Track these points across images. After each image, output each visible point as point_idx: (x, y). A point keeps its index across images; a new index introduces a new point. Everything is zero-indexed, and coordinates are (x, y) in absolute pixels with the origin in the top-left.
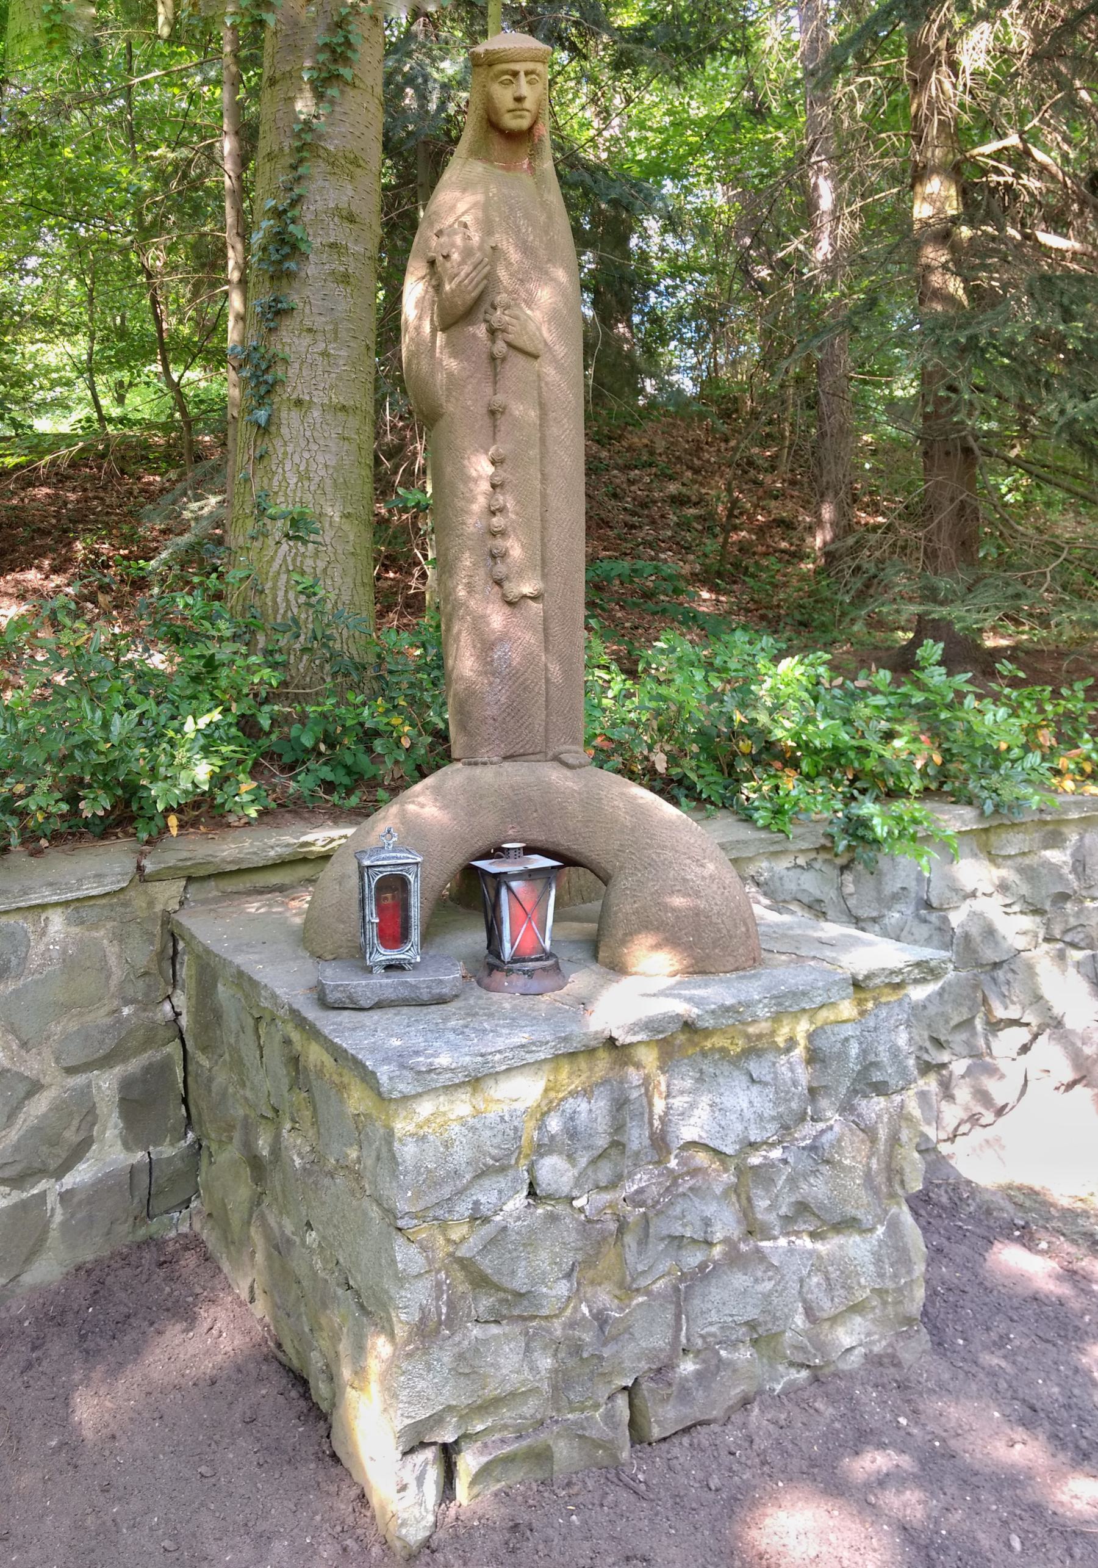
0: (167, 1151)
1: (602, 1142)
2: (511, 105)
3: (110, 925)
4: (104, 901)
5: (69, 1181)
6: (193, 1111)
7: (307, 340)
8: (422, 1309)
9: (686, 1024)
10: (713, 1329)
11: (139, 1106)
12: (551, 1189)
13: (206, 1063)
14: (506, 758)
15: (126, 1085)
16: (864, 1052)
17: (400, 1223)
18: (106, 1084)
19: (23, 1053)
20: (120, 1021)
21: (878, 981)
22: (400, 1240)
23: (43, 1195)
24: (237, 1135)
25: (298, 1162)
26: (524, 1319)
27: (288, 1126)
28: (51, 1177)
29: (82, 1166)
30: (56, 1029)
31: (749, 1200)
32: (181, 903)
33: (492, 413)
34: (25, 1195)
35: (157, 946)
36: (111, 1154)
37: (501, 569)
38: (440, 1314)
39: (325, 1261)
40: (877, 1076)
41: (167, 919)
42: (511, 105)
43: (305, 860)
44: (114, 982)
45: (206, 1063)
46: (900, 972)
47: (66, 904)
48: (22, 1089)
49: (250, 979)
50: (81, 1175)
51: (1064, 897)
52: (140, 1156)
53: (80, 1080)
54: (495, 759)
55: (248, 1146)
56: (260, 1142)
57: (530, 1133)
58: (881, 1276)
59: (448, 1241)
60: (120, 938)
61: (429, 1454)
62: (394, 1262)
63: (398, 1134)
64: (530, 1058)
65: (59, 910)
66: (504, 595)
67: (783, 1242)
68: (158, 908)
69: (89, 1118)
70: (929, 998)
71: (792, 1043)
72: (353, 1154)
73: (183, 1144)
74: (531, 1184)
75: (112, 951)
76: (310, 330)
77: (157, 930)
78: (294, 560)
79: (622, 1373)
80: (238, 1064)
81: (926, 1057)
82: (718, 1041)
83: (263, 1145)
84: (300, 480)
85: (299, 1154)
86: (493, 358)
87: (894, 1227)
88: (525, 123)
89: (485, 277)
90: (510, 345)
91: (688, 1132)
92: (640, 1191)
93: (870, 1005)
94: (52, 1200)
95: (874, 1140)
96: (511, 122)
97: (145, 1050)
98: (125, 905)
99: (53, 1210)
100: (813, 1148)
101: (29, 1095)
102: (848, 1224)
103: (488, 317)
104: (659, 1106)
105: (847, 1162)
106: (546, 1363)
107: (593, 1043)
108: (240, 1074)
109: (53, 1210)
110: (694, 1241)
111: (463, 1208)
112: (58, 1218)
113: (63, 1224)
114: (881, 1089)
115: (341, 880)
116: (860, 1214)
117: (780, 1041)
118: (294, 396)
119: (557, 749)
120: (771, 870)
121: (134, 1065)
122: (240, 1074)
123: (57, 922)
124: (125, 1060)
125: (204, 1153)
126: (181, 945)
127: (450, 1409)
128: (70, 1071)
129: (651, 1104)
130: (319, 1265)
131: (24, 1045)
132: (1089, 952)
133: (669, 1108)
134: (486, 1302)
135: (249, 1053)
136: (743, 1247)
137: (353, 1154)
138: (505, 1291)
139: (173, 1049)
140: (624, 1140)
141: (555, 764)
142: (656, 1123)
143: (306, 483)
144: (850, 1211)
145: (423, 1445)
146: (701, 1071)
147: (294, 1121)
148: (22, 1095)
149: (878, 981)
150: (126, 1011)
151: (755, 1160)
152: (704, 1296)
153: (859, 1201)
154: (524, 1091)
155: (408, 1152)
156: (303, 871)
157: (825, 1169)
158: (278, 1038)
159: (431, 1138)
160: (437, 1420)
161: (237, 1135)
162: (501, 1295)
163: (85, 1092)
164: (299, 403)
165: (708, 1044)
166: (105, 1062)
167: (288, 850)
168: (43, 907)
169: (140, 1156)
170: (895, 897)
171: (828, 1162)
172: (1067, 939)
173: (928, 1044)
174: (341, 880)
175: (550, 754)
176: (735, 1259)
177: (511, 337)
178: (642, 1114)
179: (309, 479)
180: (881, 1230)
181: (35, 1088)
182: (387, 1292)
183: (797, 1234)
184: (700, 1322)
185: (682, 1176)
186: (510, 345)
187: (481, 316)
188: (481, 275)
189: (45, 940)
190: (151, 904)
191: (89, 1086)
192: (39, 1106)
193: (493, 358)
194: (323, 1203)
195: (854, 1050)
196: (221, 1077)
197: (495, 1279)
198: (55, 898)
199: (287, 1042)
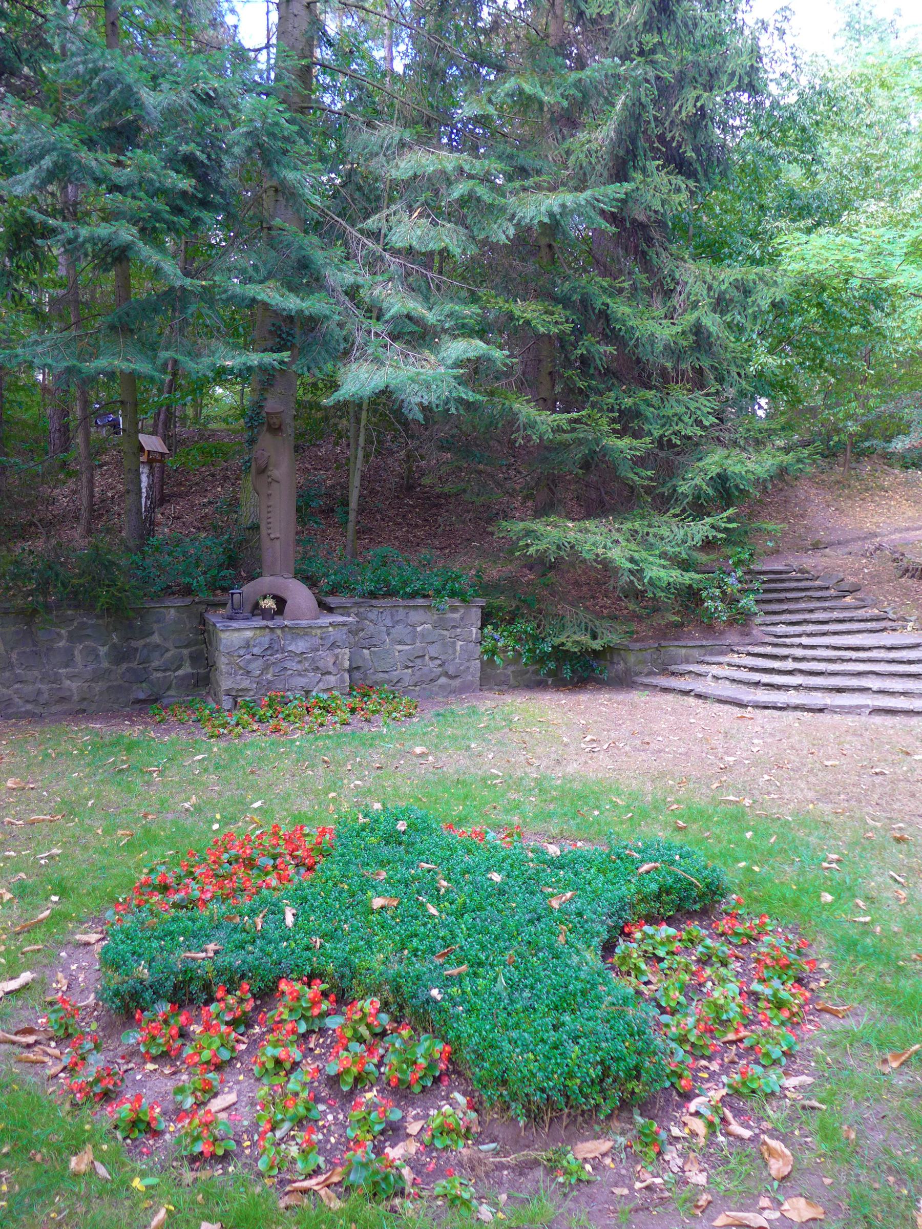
5: (177, 674)
15: (191, 653)
36: (187, 669)
50: (180, 672)
102: (329, 673)
121: (193, 649)
123: (172, 611)
155: (224, 641)
166: (186, 647)
181: (167, 650)
192: (168, 655)
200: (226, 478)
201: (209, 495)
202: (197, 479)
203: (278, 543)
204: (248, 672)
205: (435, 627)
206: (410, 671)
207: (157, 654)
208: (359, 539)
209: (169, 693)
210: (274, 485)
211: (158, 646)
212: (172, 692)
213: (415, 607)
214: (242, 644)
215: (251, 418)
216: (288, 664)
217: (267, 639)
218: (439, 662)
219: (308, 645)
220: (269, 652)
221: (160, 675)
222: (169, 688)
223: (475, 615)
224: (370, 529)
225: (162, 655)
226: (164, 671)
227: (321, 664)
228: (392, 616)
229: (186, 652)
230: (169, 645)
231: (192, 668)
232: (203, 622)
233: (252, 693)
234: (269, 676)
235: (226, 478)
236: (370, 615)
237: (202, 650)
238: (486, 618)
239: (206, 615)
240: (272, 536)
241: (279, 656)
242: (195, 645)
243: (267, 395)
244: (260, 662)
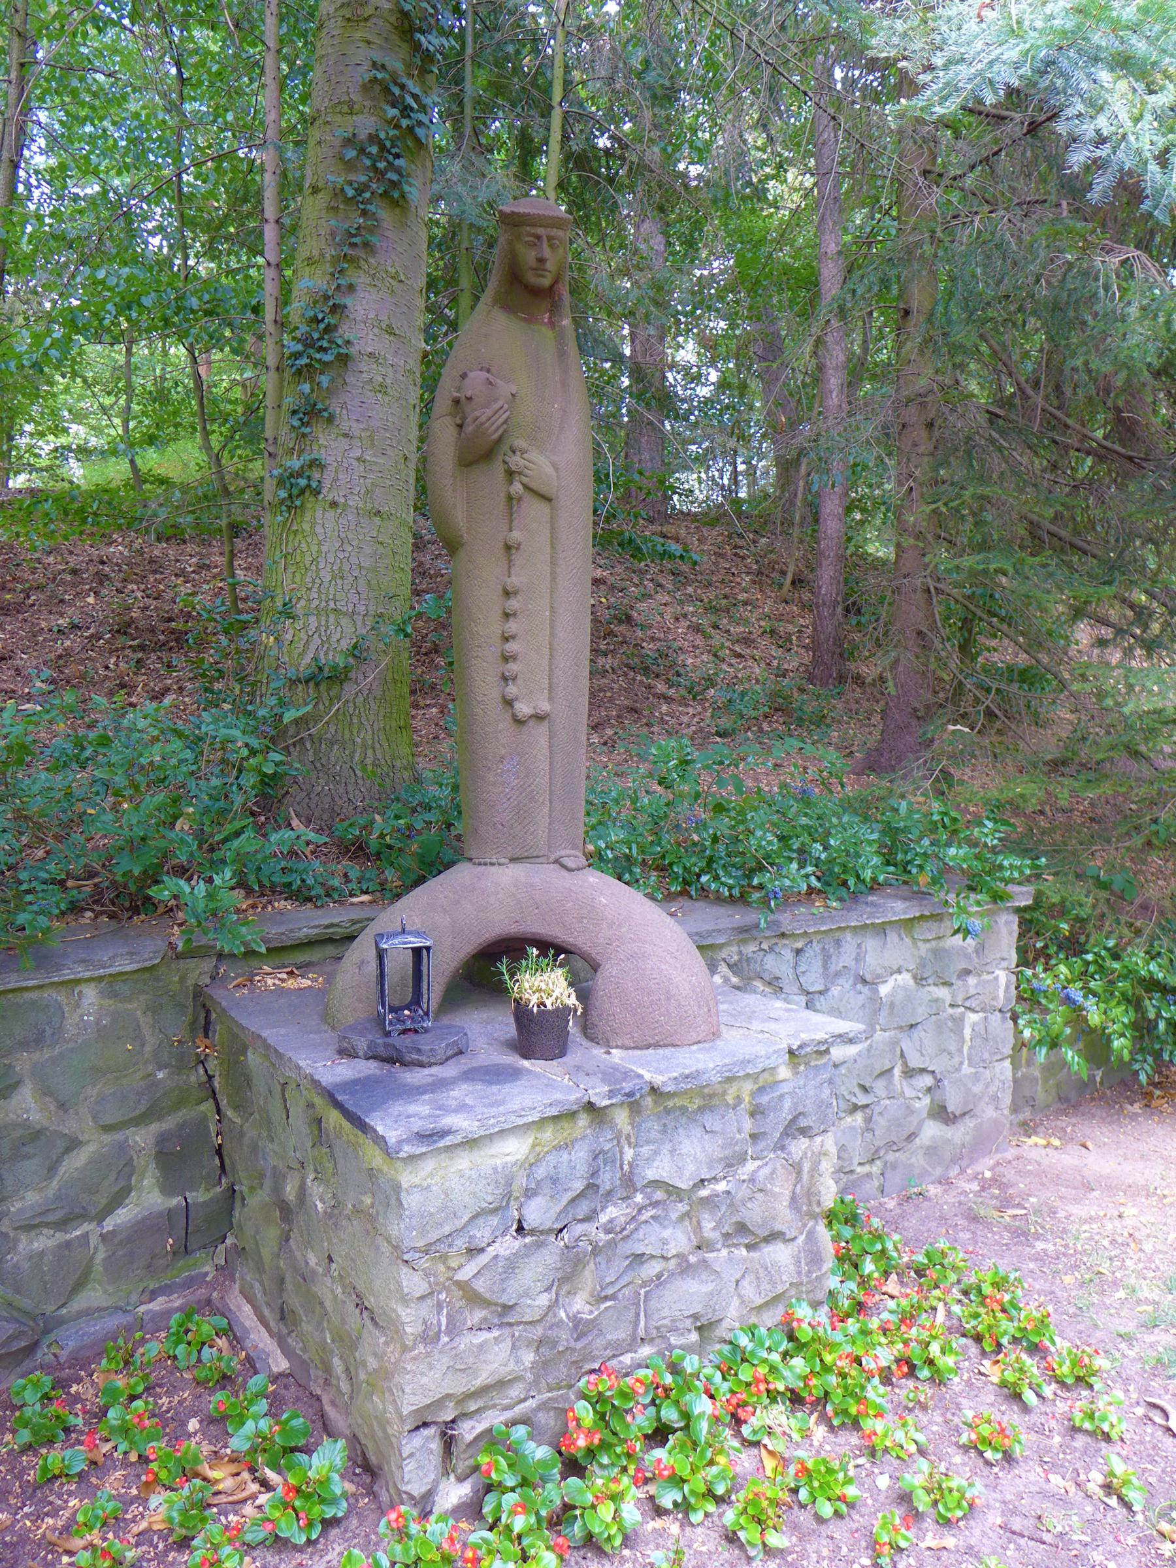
0: (199, 1196)
1: (579, 1186)
2: (534, 264)
3: (142, 998)
4: (136, 976)
5: (109, 1225)
6: (227, 1161)
7: (344, 443)
8: (425, 1322)
9: (653, 1088)
10: (665, 1322)
11: (173, 1160)
12: (535, 1224)
13: (238, 1120)
14: (512, 860)
15: (162, 1139)
16: (795, 1105)
17: (406, 1257)
18: (142, 1138)
19: (61, 1113)
20: (157, 1084)
21: (808, 1049)
22: (405, 1270)
23: (86, 1235)
24: (268, 1183)
25: (320, 1205)
26: (511, 1325)
27: (311, 1177)
28: (92, 1220)
29: (121, 1211)
30: (93, 1092)
31: (699, 1223)
32: (213, 978)
33: (508, 548)
34: (68, 1237)
35: (190, 1018)
36: (149, 1198)
37: (512, 690)
38: (440, 1325)
39: (344, 1287)
40: (803, 1122)
41: (198, 992)
42: (534, 264)
43: (331, 940)
44: (148, 1048)
45: (238, 1120)
46: (826, 1042)
47: (100, 979)
48: (61, 1144)
49: (276, 1051)
50: (122, 1216)
51: (967, 972)
52: (176, 1201)
53: (118, 1136)
54: (503, 860)
55: (277, 1190)
56: (288, 1188)
57: (521, 1182)
58: (799, 1273)
59: (449, 1268)
60: (153, 1009)
61: (431, 1431)
62: (401, 1287)
63: (405, 1185)
64: (520, 1121)
65: (93, 985)
66: (514, 716)
67: (724, 1252)
68: (190, 982)
69: (127, 1169)
70: (859, 1054)
71: (739, 1099)
72: (368, 1200)
73: (218, 1189)
74: (519, 1221)
75: (145, 1021)
76: (346, 435)
77: (190, 1002)
78: (326, 653)
79: (593, 1360)
80: (267, 1122)
81: (854, 1100)
82: (678, 1102)
83: (290, 1191)
84: (334, 578)
85: (321, 1200)
86: (510, 498)
87: (811, 1236)
88: (546, 282)
89: (505, 422)
90: (525, 486)
91: (651, 1174)
92: (611, 1221)
93: (802, 1068)
94: (94, 1240)
95: (799, 1173)
96: (532, 279)
97: (179, 1109)
98: (157, 979)
99: (96, 1248)
100: (752, 1180)
101: (68, 1150)
102: (774, 1236)
103: (507, 459)
104: (629, 1154)
105: (777, 1190)
106: (528, 1357)
107: (575, 1107)
108: (269, 1130)
109: (96, 1248)
110: (652, 1257)
111: (461, 1243)
112: (101, 1256)
113: (104, 1260)
114: (804, 1132)
115: (361, 964)
116: (784, 1228)
117: (730, 1099)
118: (330, 498)
119: (559, 854)
120: (740, 953)
121: (169, 1124)
122: (269, 1130)
123: (90, 994)
124: (160, 1118)
125: (238, 1195)
126: (214, 1016)
127: (448, 1396)
128: (108, 1129)
129: (621, 1153)
130: (339, 1290)
131: (62, 1106)
132: (981, 1015)
133: (637, 1155)
134: (479, 1315)
135: (277, 1113)
136: (692, 1259)
137: (368, 1200)
138: (496, 1304)
139: (208, 1107)
140: (598, 1182)
141: (557, 866)
142: (626, 1167)
143: (339, 582)
144: (778, 1227)
145: (425, 1425)
146: (665, 1125)
147: (316, 1171)
148: (61, 1150)
149: (808, 1049)
150: (160, 1075)
151: (704, 1193)
152: (659, 1297)
153: (785, 1218)
154: (515, 1149)
155: (412, 1201)
156: (330, 950)
157: (760, 1196)
158: (302, 1103)
159: (434, 1188)
160: (439, 1404)
161: (268, 1183)
162: (493, 1308)
163: (122, 1147)
164: (334, 504)
165: (670, 1104)
166: (140, 1120)
167: (316, 931)
168: (78, 982)
169: (176, 1201)
170: (838, 974)
171: (761, 1190)
172: (967, 1004)
173: (857, 1090)
174: (361, 964)
175: (552, 859)
176: (685, 1268)
177: (525, 480)
178: (614, 1161)
179: (342, 578)
180: (801, 1239)
181: (74, 1144)
182: (395, 1311)
183: (736, 1246)
184: (656, 1317)
185: (645, 1207)
186: (525, 486)
187: (501, 458)
188: (501, 420)
189: (80, 1011)
190: (183, 979)
191: (126, 1141)
192: (79, 1159)
193: (510, 498)
194: (342, 1241)
195: (787, 1104)
196: (251, 1133)
197: (487, 1296)
198: (88, 974)
199: (310, 1105)
200: (101, 578)
201: (70, 611)
202: (39, 578)
203: (539, 735)
204: (507, 1309)
205: (920, 980)
206: (859, 1117)
207: (32, 1167)
208: (415, 706)
209: (80, 1302)
210: (534, 510)
211: (37, 1134)
212: (94, 1296)
213: (881, 930)
214: (489, 1195)
215: (308, 343)
216: (648, 1240)
217: (580, 1155)
218: (928, 1080)
219: (713, 1148)
220: (583, 1209)
221: (45, 1241)
222: (79, 1286)
223: (1007, 929)
224: (433, 687)
225: (52, 1169)
226: (62, 1225)
227: (753, 1214)
228: (827, 959)
229: (142, 1138)
230: (80, 1124)
231: (167, 1190)
232: (204, 1015)
233: (515, 1392)
234: (580, 1304)
235: (101, 578)
236: (770, 962)
237: (204, 1120)
238: (1039, 939)
239: (217, 993)
240: (523, 709)
241: (612, 1212)
242: (179, 1104)
243: (360, 279)
244: (549, 1257)
